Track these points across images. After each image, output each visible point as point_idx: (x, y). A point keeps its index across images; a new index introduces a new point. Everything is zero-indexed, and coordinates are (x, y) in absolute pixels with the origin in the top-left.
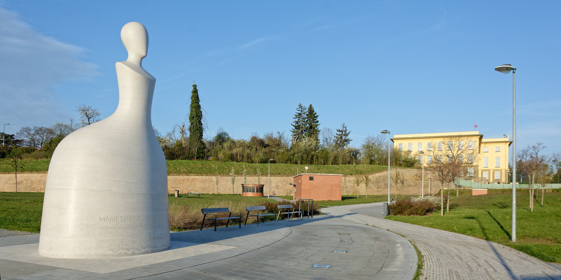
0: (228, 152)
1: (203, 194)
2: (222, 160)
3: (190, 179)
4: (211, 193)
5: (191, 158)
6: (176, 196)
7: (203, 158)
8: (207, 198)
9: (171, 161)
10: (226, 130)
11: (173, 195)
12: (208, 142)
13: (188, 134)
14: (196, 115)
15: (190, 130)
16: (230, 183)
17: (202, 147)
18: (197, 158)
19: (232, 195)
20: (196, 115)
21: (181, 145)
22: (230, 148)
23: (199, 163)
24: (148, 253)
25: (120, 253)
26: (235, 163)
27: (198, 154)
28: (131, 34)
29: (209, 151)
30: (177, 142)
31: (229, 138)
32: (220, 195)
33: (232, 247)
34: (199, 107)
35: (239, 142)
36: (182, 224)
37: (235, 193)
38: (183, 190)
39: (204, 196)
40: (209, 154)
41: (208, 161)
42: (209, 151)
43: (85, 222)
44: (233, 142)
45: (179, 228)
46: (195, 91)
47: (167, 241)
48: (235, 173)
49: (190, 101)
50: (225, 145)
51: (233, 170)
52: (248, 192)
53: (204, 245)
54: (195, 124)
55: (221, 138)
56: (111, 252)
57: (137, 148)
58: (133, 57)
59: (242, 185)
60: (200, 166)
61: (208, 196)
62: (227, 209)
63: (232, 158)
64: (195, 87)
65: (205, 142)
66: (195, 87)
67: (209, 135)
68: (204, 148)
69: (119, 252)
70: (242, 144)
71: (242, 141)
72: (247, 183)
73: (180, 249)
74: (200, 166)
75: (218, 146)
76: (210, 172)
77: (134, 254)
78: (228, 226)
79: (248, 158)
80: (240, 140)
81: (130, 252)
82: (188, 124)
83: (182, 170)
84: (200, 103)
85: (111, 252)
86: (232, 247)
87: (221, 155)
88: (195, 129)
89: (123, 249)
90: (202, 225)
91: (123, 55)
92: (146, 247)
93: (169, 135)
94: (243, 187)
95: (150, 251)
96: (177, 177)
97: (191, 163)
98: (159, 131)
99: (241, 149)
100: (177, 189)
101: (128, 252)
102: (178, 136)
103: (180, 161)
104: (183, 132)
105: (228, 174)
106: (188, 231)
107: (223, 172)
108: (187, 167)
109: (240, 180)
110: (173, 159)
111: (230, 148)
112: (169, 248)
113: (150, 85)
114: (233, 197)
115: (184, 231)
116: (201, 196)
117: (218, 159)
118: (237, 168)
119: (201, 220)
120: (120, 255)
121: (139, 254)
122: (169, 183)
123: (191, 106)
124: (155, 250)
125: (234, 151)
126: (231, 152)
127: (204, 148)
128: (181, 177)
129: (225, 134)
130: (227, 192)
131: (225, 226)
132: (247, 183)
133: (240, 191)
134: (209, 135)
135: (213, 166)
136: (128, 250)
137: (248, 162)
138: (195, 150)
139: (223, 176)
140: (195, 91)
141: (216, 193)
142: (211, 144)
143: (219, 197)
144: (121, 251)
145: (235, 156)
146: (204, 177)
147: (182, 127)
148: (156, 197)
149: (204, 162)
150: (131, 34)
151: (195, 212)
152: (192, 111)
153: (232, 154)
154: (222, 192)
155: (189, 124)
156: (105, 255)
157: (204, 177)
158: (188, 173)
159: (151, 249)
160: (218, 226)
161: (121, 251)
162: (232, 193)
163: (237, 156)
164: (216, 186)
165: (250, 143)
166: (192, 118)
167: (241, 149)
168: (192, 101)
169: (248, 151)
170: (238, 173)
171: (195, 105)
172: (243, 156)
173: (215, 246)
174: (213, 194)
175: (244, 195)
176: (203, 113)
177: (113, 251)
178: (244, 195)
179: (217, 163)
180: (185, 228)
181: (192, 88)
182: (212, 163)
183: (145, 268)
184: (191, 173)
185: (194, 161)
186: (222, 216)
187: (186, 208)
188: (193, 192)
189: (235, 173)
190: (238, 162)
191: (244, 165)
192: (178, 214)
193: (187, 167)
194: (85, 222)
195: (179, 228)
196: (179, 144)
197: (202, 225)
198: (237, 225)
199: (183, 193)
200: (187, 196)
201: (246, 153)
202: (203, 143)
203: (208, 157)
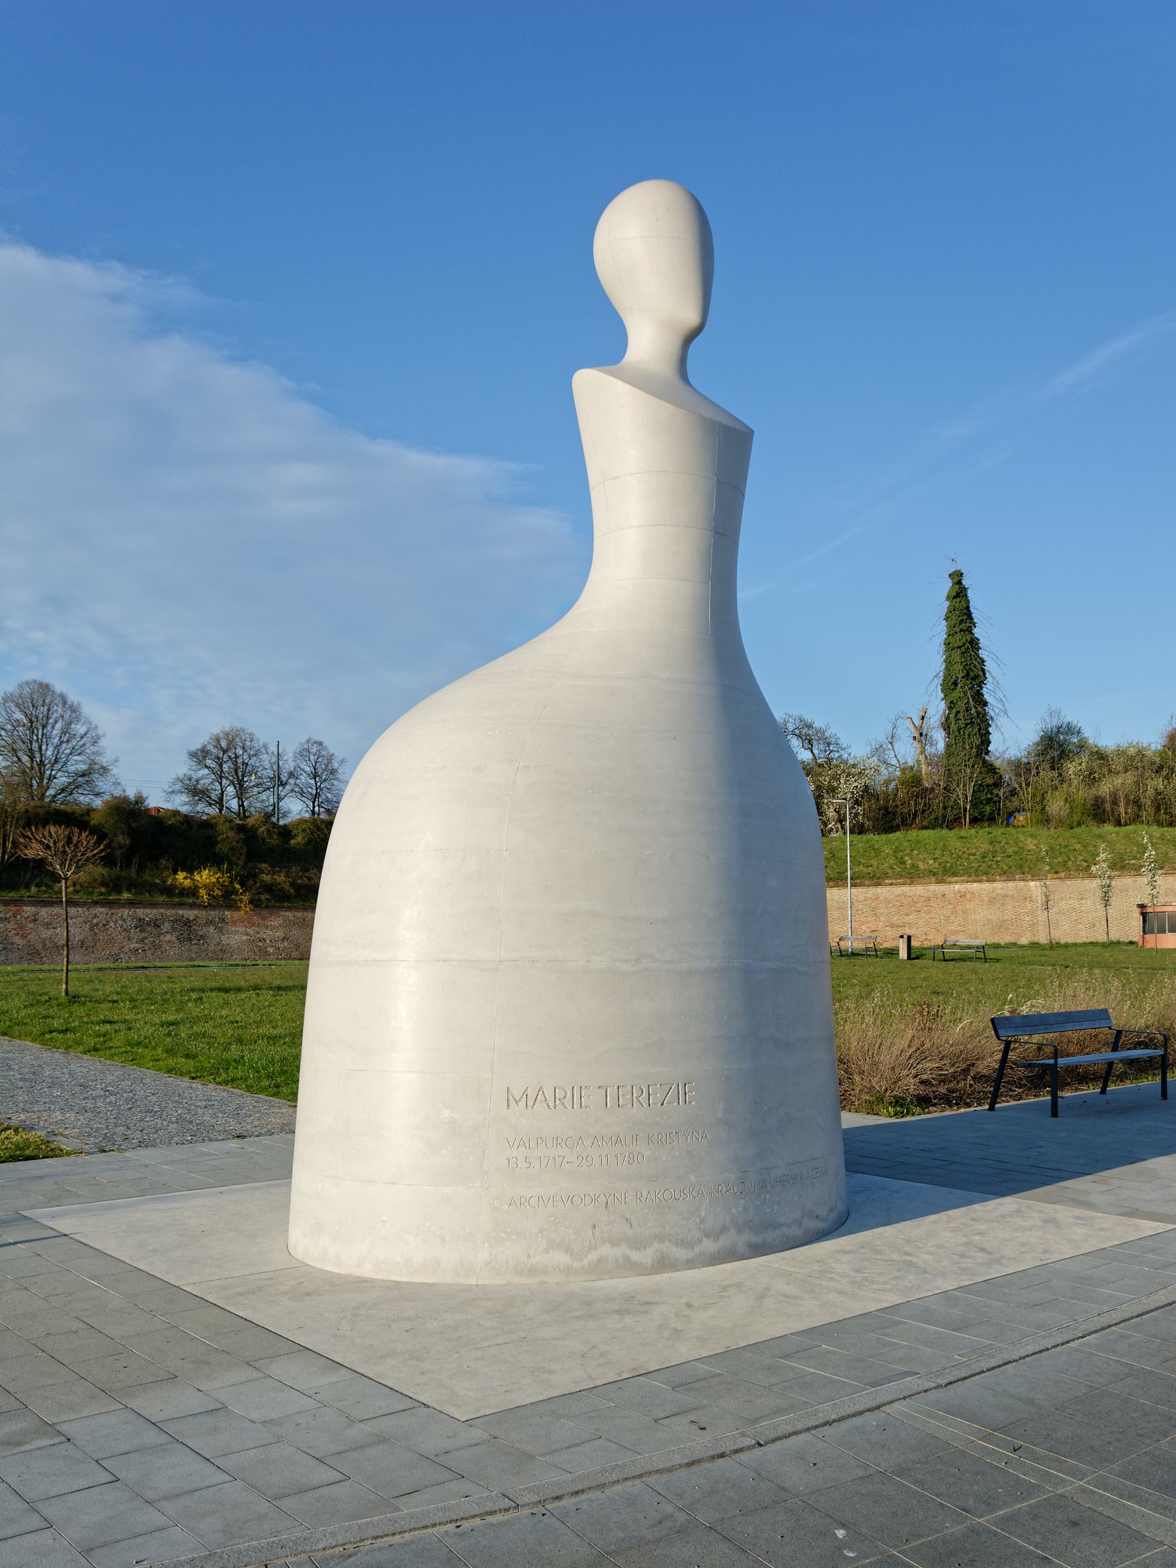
0: (1083, 794)
1: (997, 946)
2: (1061, 822)
3: (950, 896)
4: (1024, 941)
5: (952, 823)
6: (903, 954)
7: (992, 819)
8: (1011, 959)
9: (884, 837)
10: (1071, 716)
11: (892, 953)
12: (1010, 762)
13: (939, 741)
14: (966, 674)
15: (946, 726)
16: (1092, 906)
17: (990, 781)
18: (974, 821)
19: (1104, 945)
20: (966, 674)
21: (916, 780)
22: (1091, 779)
23: (979, 838)
24: (731, 1255)
25: (601, 1260)
26: (1108, 828)
27: (974, 805)
28: (639, 245)
29: (1013, 793)
30: (903, 771)
31: (1082, 745)
32: (1058, 945)
33: (1150, 1227)
34: (974, 644)
35: (1120, 752)
36: (911, 1085)
37: (1114, 937)
38: (927, 935)
39: (1000, 953)
40: (1015, 802)
41: (1011, 830)
42: (1013, 793)
43: (446, 1113)
44: (1101, 756)
45: (899, 1103)
46: (959, 593)
47: (826, 1190)
48: (1113, 866)
49: (941, 630)
50: (1071, 768)
51: (1103, 856)
52: (1162, 931)
53: (1008, 1203)
54: (961, 706)
55: (1056, 747)
56: (560, 1258)
57: (672, 759)
58: (648, 340)
59: (1142, 906)
60: (986, 847)
61: (1013, 952)
62: (1103, 1014)
63: (1099, 812)
64: (957, 578)
65: (997, 764)
66: (957, 578)
67: (1012, 738)
68: (997, 784)
69: (593, 1256)
70: (1135, 761)
71: (1132, 751)
72: (1162, 899)
73: (889, 1230)
74: (986, 847)
75: (1047, 774)
76: (1022, 867)
77: (663, 1264)
78: (1111, 1088)
79: (1158, 809)
80: (1124, 744)
81: (646, 1256)
82: (938, 708)
83: (921, 865)
84: (977, 632)
85: (560, 1258)
86: (1150, 1227)
87: (1056, 806)
88: (962, 723)
89: (614, 1242)
90: (997, 1084)
91: (605, 341)
92: (723, 1230)
93: (878, 750)
94: (1144, 915)
95: (741, 1248)
96: (906, 888)
97: (951, 837)
98: (844, 742)
99: (1130, 778)
100: (908, 932)
101: (636, 1256)
102: (906, 752)
103: (914, 834)
104: (921, 736)
105: (1085, 871)
106: (935, 1114)
107: (1068, 864)
108: (938, 852)
109: (1132, 890)
110: (891, 829)
111: (1091, 779)
112: (839, 1225)
113: (726, 460)
114: (1105, 956)
115: (918, 1117)
116: (991, 954)
117: (1046, 821)
118: (1120, 847)
119: (990, 1063)
120: (599, 1269)
121: (690, 1264)
122: (832, 914)
123: (947, 644)
124: (766, 1239)
125: (1105, 788)
126: (1093, 791)
127: (997, 784)
128: (918, 890)
129: (1070, 730)
130: (1083, 937)
131: (1092, 1090)
132: (1162, 899)
133: (1132, 929)
134: (1012, 738)
135: (1031, 844)
136: (639, 1244)
137: (1160, 824)
138: (963, 794)
139: (1068, 877)
140: (959, 593)
141: (1043, 940)
142: (1022, 768)
143: (1060, 957)
144: (606, 1250)
145: (1108, 807)
146: (999, 886)
147: (917, 722)
148: (768, 981)
149: (997, 831)
150: (639, 245)
151: (966, 1029)
152: (949, 663)
153: (1097, 798)
154: (1065, 933)
155: (942, 706)
156: (533, 1271)
157: (998, 885)
158: (944, 874)
159: (749, 1236)
160: (1064, 1085)
161: (606, 1250)
162: (1101, 938)
163: (1115, 802)
164: (1042, 916)
165: (1161, 754)
166: (949, 686)
167: (1130, 778)
168: (950, 627)
169: (1159, 783)
170: (1120, 865)
171: (959, 639)
172: (1137, 803)
173: (1063, 1213)
174: (1034, 945)
175: (1148, 946)
176: (989, 666)
177: (568, 1250)
178: (1148, 946)
179: (1044, 832)
180: (924, 1102)
181: (947, 585)
182: (1027, 836)
183: (689, 1382)
184: (955, 874)
185: (963, 833)
186: (1082, 1049)
187: (929, 1017)
188: (963, 940)
189: (1113, 866)
190: (1118, 823)
191: (1145, 833)
192: (888, 1039)
193: (938, 852)
194: (446, 1113)
195: (899, 1103)
196: (912, 780)
197: (997, 1084)
198: (1151, 1082)
199: (927, 944)
200: (939, 956)
201: (1150, 792)
202: (991, 769)
203: (1010, 814)
